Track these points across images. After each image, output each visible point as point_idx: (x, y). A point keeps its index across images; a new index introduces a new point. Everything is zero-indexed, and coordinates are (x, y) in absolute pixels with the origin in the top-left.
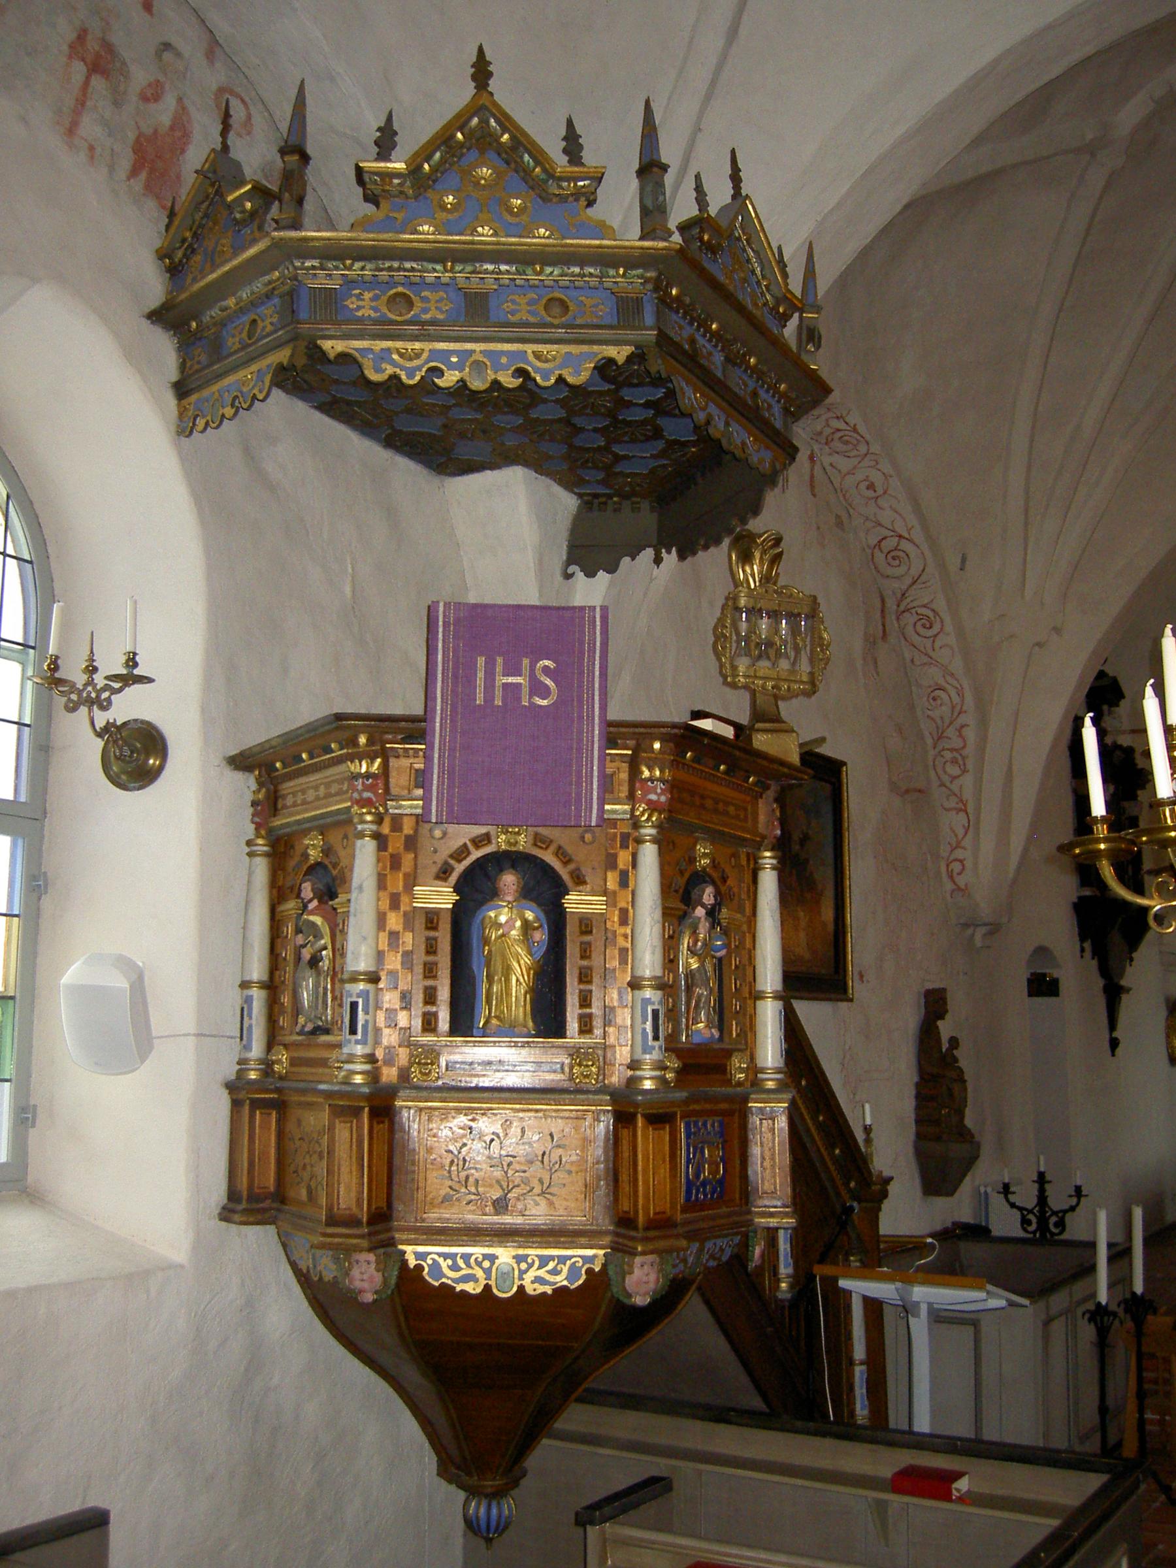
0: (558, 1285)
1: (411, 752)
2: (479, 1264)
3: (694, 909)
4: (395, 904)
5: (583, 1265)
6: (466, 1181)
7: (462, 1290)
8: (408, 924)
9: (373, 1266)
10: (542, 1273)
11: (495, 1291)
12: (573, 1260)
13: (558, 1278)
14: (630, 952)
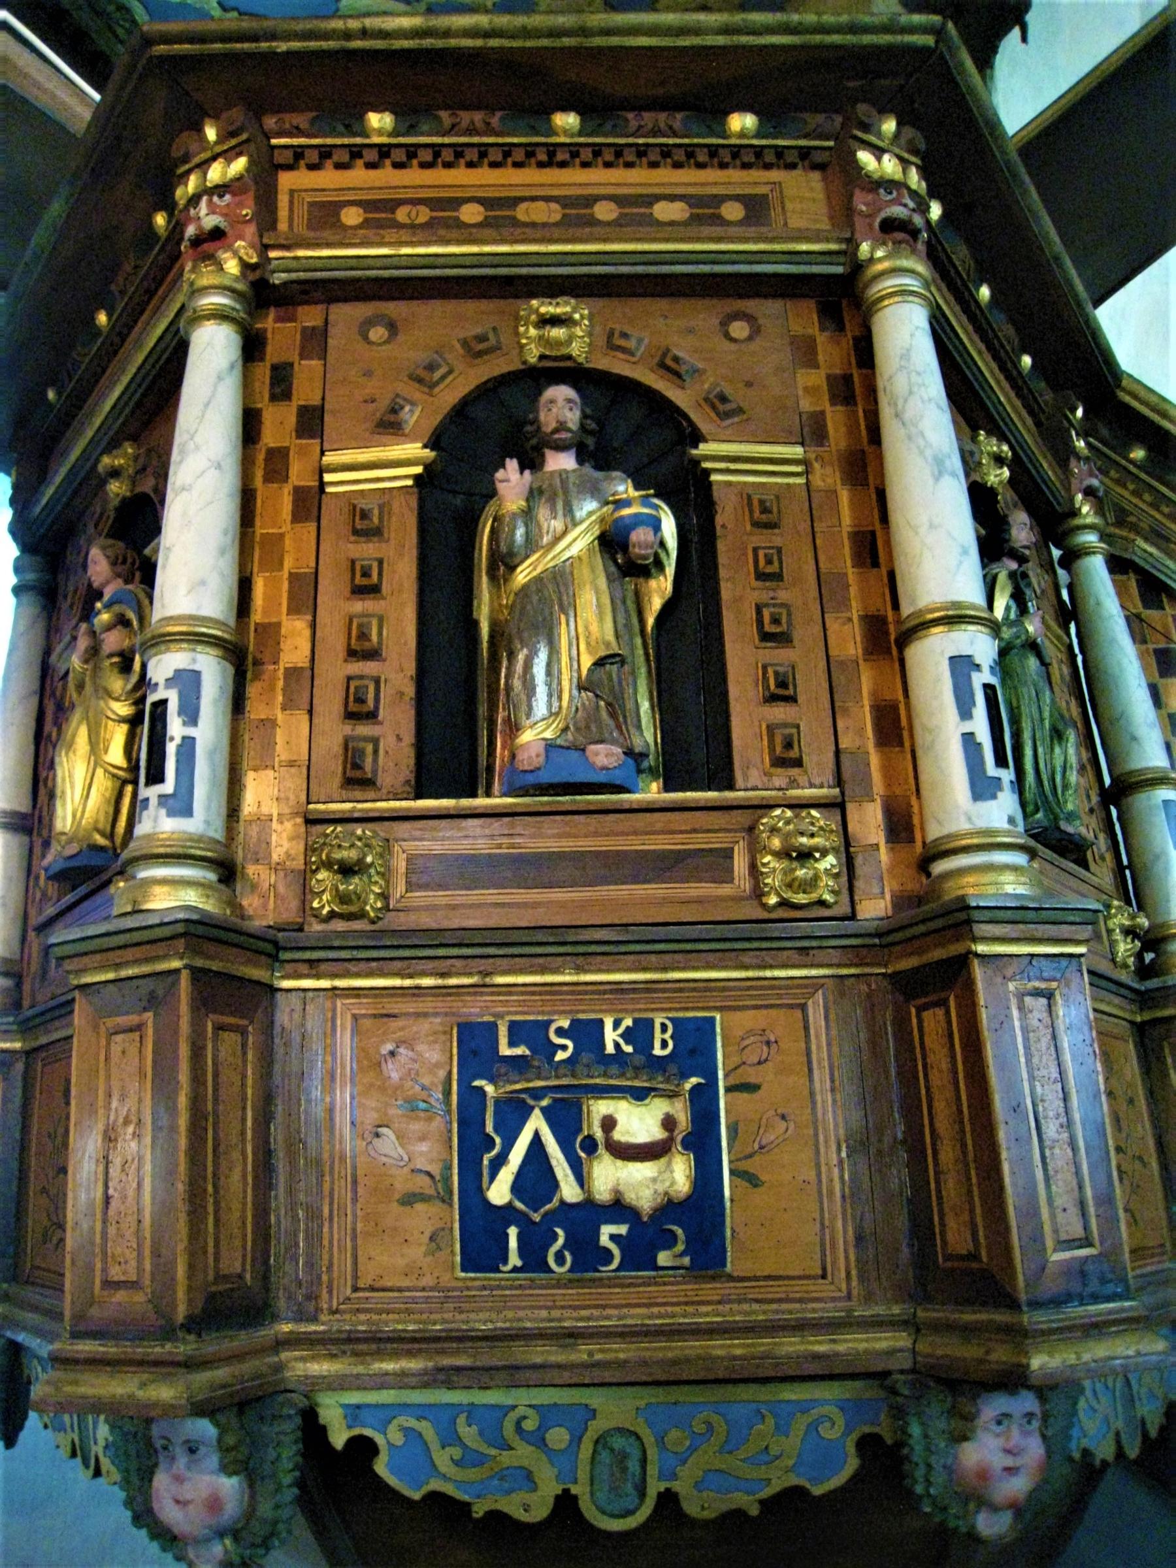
1: (733, 211)
2: (538, 1440)
11: (587, 1508)
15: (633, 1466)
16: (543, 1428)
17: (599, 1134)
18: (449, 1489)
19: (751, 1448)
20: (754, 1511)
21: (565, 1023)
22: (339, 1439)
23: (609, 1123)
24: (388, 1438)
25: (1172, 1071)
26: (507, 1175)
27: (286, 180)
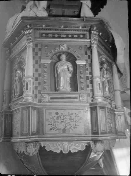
0: (79, 150)
1: (82, 36)
2: (59, 145)
4: (37, 62)
6: (55, 125)
8: (40, 66)
9: (32, 146)
10: (75, 147)
11: (64, 152)
12: (82, 143)
13: (79, 148)
18: (52, 150)
20: (77, 152)
22: (42, 146)
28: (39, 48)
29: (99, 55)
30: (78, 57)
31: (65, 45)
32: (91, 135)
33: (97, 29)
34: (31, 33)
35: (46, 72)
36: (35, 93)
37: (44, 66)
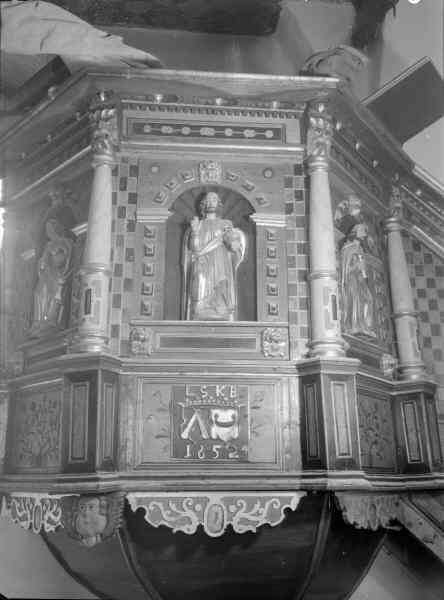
1: (269, 134)
3: (96, 359)
5: (281, 506)
7: (180, 532)
10: (247, 516)
14: (177, 322)
15: (220, 516)
16: (195, 504)
17: (213, 419)
19: (253, 512)
20: (254, 531)
21: (205, 387)
22: (134, 509)
23: (216, 416)
24: (149, 508)
25: (8, 278)
26: (187, 430)
27: (125, 112)
28: (130, 194)
29: (337, 196)
30: (259, 200)
31: (216, 162)
32: (300, 473)
33: (329, 113)
34: (112, 117)
35: (152, 234)
36: (115, 262)
37: (147, 231)
